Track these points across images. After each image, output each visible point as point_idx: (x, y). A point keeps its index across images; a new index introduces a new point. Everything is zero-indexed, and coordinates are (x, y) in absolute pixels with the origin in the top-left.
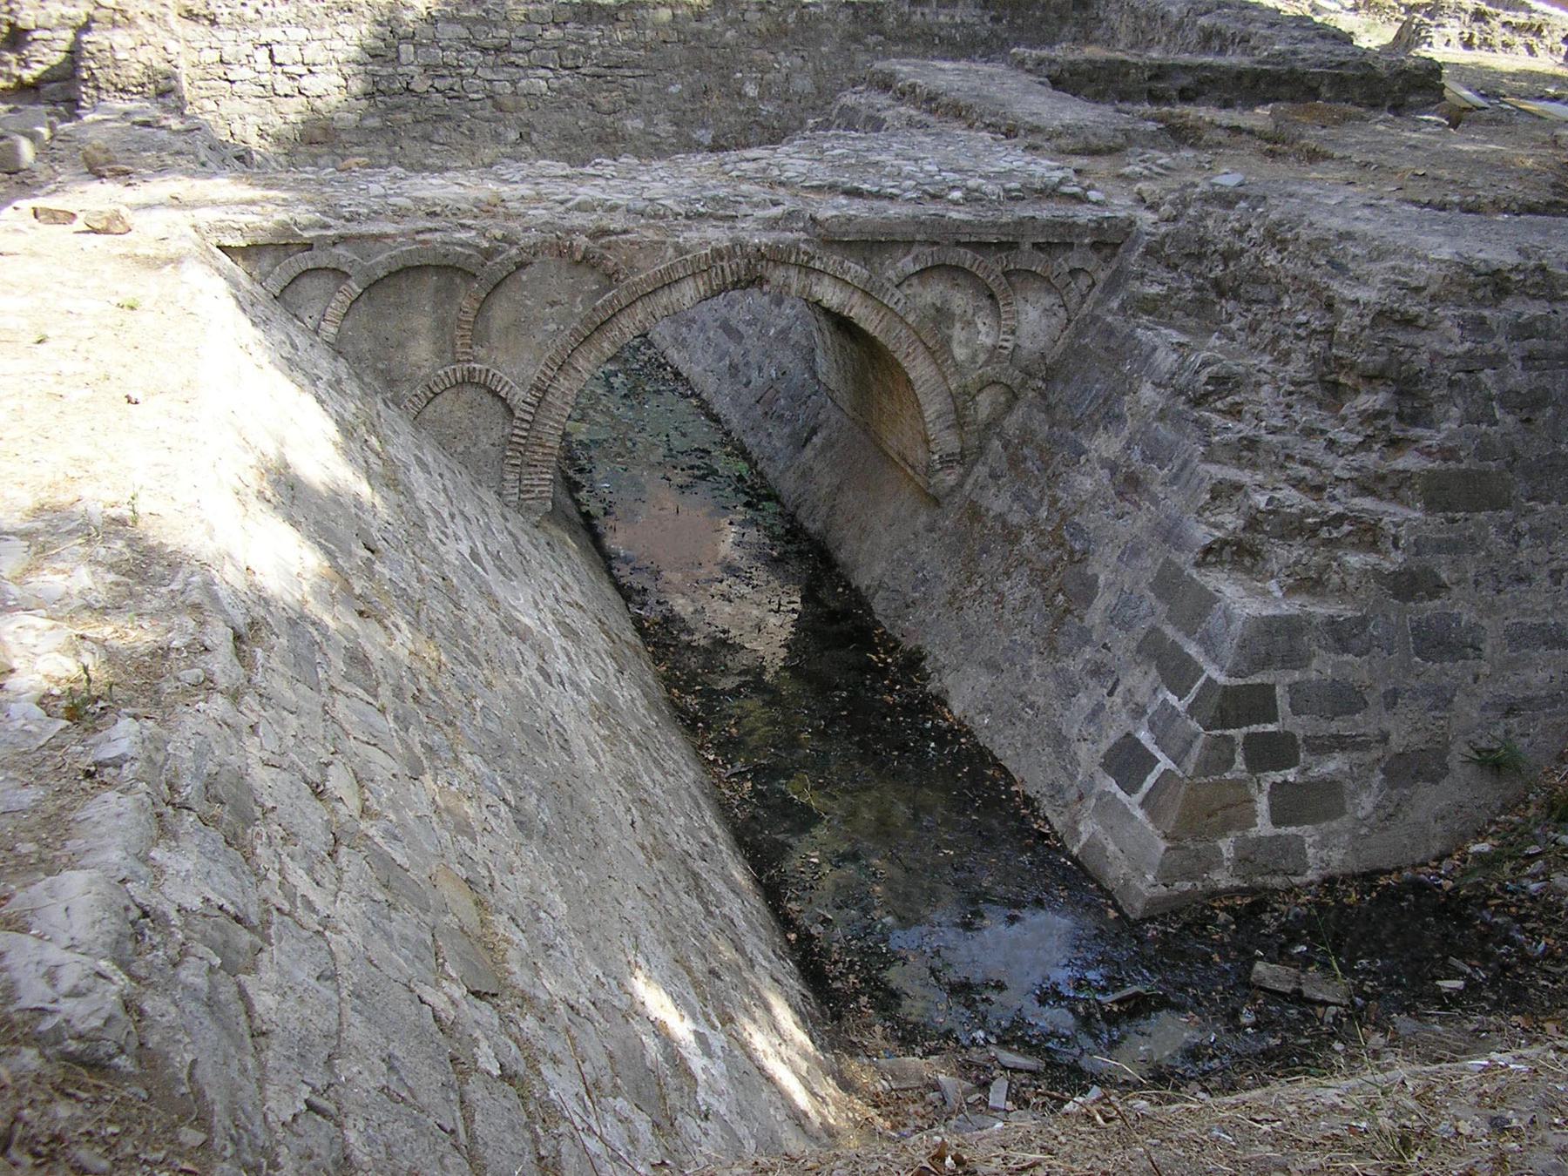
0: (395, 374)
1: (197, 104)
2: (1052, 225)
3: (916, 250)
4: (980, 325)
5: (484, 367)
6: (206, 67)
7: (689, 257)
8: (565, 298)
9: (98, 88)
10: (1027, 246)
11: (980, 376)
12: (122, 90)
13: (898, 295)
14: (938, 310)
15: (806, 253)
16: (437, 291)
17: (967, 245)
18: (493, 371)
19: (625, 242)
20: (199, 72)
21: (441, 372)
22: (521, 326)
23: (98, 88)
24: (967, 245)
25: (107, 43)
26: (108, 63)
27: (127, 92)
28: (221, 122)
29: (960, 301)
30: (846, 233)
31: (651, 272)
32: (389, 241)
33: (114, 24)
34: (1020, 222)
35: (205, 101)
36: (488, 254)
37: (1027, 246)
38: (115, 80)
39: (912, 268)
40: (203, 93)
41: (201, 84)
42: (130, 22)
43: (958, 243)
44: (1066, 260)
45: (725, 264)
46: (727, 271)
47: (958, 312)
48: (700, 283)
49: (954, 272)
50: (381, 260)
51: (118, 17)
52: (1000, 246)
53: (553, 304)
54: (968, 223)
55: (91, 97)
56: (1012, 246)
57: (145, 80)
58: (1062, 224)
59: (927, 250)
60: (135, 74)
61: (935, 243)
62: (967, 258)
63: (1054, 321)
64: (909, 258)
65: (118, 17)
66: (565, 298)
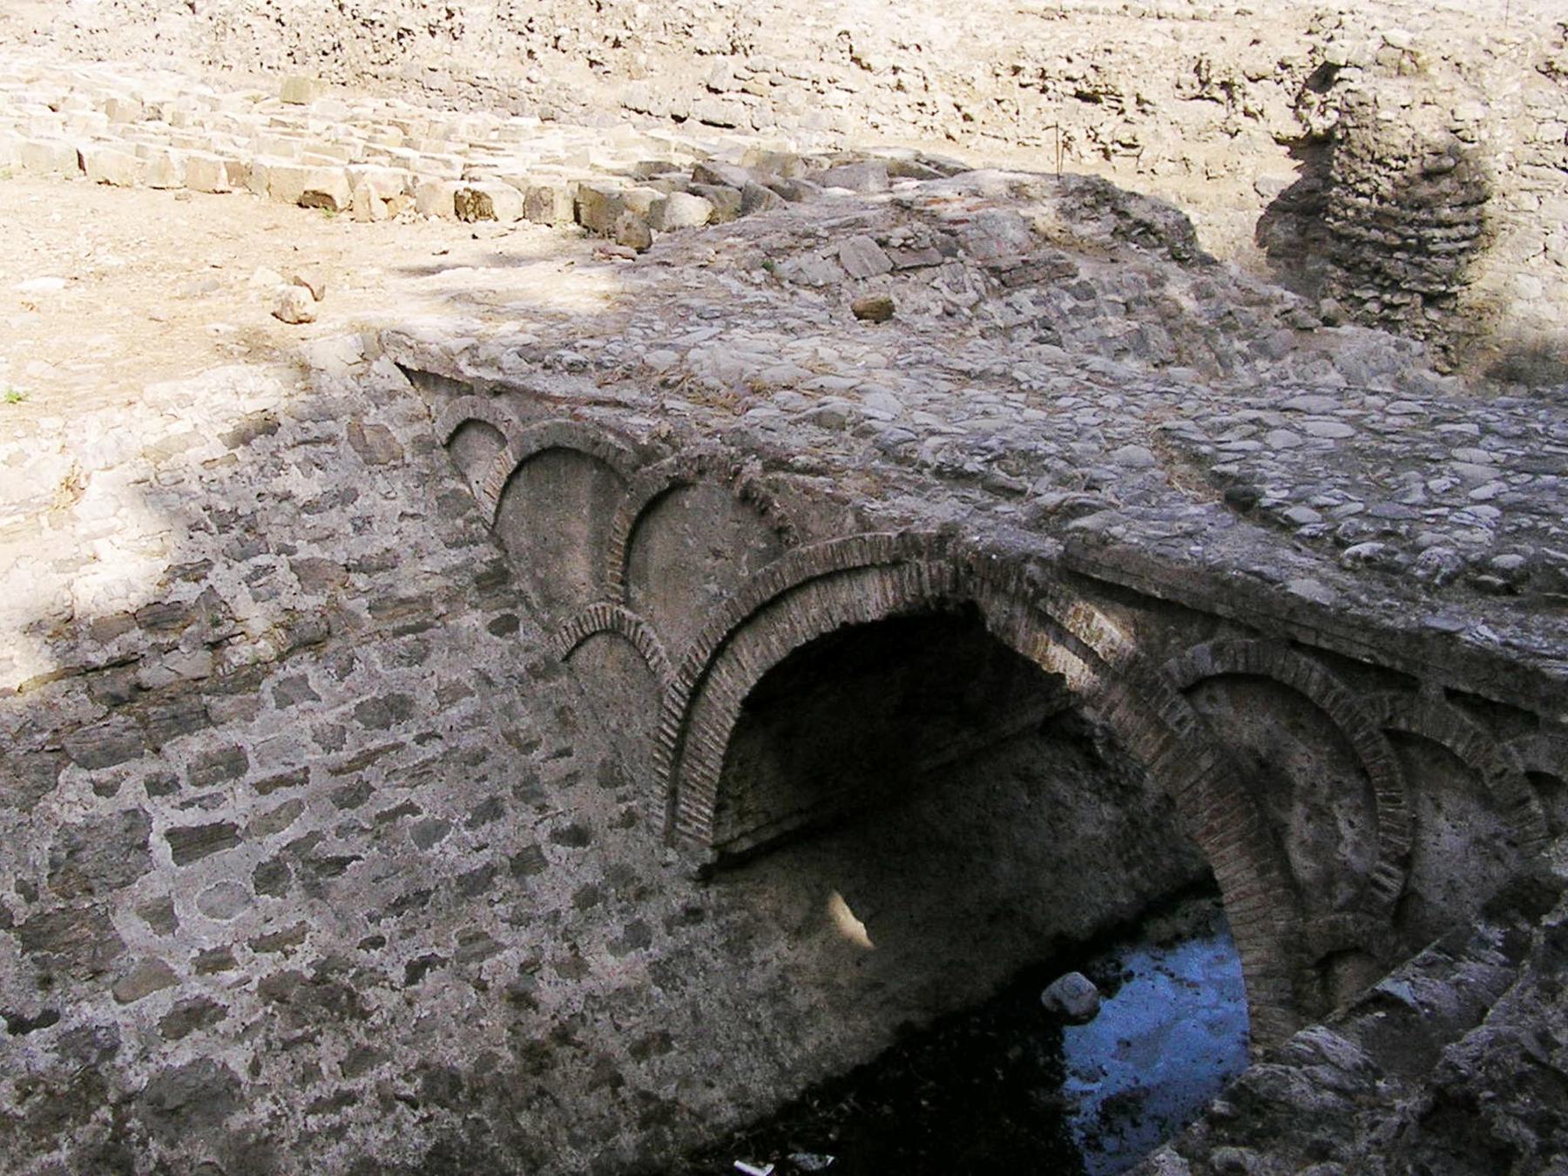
0: (553, 590)
1: (1513, 197)
2: (1484, 659)
3: (1223, 634)
4: (1342, 825)
5: (634, 617)
6: (1541, 146)
7: (867, 535)
8: (728, 550)
9: (1351, 155)
10: (1433, 692)
11: (1333, 926)
12: (1379, 162)
13: (1185, 709)
14: (1262, 764)
15: (1032, 583)
16: (596, 490)
17: (1317, 652)
18: (644, 627)
19: (797, 485)
20: (1530, 152)
21: (592, 607)
22: (678, 572)
23: (1351, 155)
24: (1317, 652)
25: (1371, 95)
26: (1366, 121)
27: (1386, 165)
28: (1536, 229)
29: (1304, 761)
30: (1095, 565)
31: (820, 544)
32: (550, 405)
33: (1400, 71)
34: (1416, 637)
35: (1525, 195)
36: (647, 455)
37: (1433, 692)
38: (1373, 146)
39: (1210, 666)
40: (1526, 183)
41: (1527, 169)
42: (1420, 70)
43: (1295, 644)
44: (1521, 749)
45: (922, 563)
46: (926, 575)
47: (1300, 780)
48: (889, 585)
49: (1290, 697)
50: (545, 426)
51: (1406, 61)
52: (1386, 676)
53: (717, 554)
54: (1314, 607)
55: (1342, 165)
56: (1407, 683)
57: (1408, 152)
58: (1511, 666)
59: (1239, 640)
60: (1397, 141)
61: (1253, 632)
62: (1313, 676)
63: (1496, 870)
64: (1206, 646)
65: (1406, 61)
66: (728, 550)
